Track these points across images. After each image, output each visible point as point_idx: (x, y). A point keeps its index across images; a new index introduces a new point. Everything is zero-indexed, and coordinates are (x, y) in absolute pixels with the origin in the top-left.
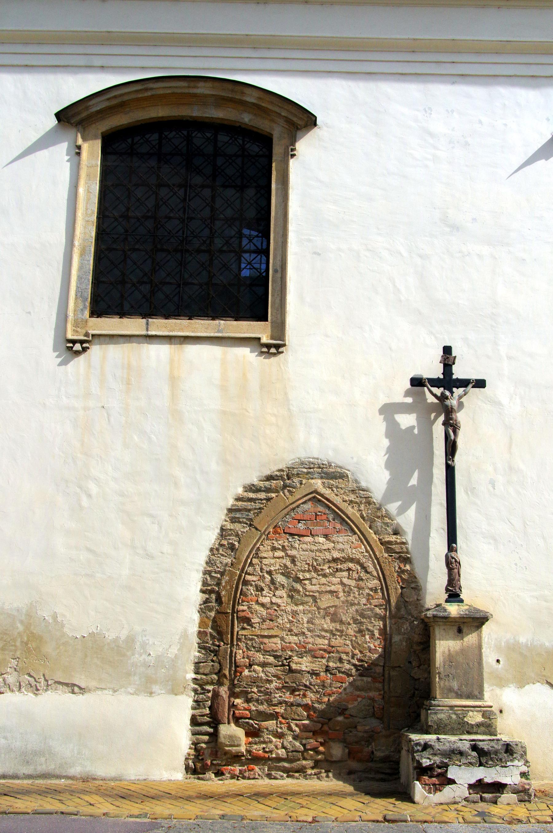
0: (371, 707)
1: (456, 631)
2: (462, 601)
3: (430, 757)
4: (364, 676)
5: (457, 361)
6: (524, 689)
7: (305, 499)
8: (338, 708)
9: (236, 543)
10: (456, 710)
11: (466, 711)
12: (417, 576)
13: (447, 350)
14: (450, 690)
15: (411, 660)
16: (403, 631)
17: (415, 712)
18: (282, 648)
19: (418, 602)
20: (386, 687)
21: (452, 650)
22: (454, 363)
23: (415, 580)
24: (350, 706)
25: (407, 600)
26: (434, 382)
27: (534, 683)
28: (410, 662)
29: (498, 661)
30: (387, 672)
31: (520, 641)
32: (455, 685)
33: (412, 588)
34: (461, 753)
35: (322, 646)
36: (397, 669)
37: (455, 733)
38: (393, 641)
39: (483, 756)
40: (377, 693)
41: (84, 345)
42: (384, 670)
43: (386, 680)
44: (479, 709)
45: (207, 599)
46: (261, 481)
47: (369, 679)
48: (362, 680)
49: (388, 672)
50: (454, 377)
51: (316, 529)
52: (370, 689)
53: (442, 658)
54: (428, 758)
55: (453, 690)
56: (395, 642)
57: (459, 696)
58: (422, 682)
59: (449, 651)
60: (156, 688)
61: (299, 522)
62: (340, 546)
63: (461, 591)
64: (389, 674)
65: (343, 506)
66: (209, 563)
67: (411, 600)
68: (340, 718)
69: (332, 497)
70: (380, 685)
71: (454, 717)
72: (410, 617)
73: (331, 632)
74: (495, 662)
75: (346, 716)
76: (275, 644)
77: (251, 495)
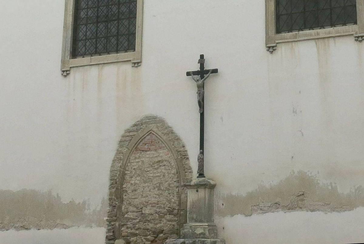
1: (196, 191)
4: (170, 215)
5: (198, 61)
7: (148, 133)
9: (122, 157)
12: (191, 166)
13: (202, 57)
14: (193, 219)
18: (140, 203)
24: (165, 229)
27: (238, 214)
29: (223, 204)
32: (195, 216)
36: (183, 210)
41: (68, 72)
42: (178, 211)
45: (112, 183)
46: (131, 127)
47: (173, 216)
48: (170, 217)
50: (199, 70)
60: (93, 225)
61: (146, 145)
66: (112, 166)
69: (158, 132)
71: (191, 231)
73: (158, 195)
76: (136, 202)
77: (128, 134)
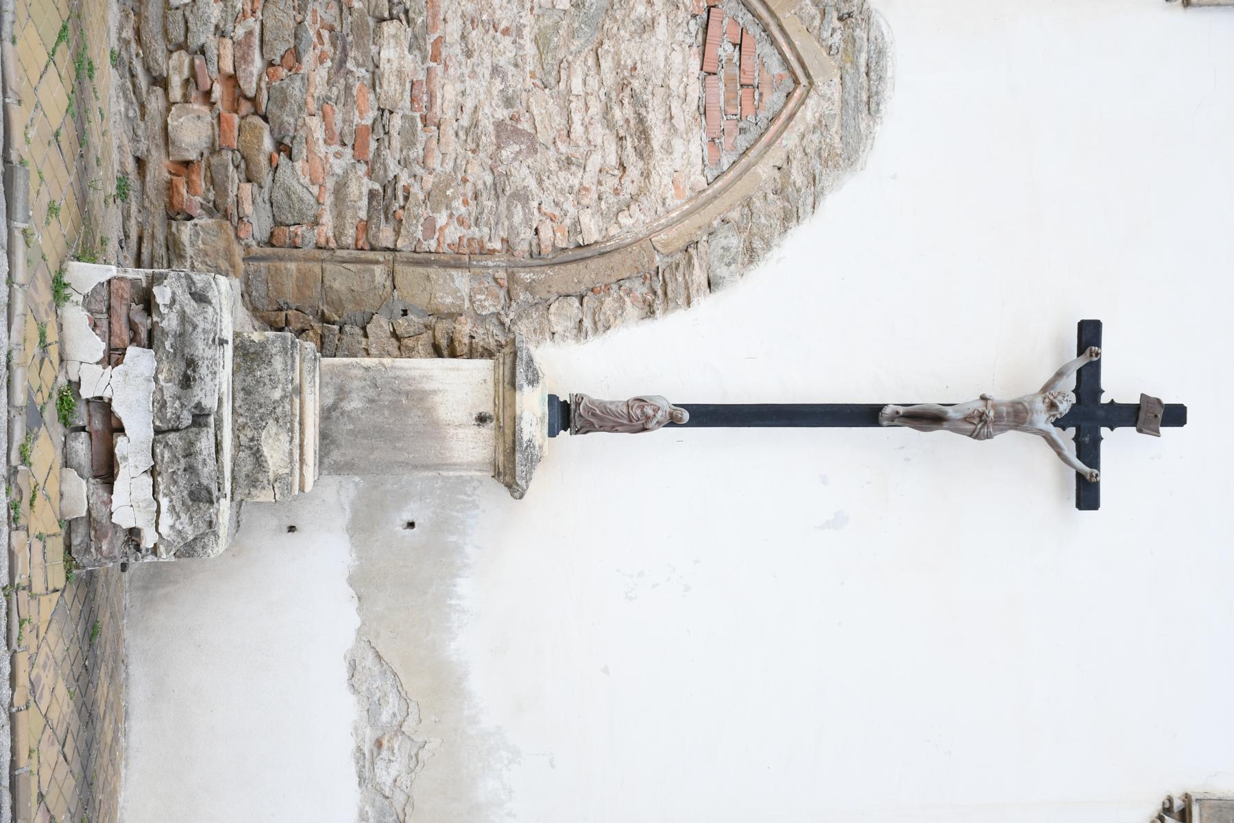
0: (297, 220)
1: (482, 409)
2: (552, 433)
3: (177, 306)
6: (346, 586)
8: (294, 138)
10: (292, 400)
11: (292, 425)
13: (1176, 415)
15: (411, 316)
16: (479, 297)
17: (287, 323)
19: (547, 335)
20: (344, 253)
21: (437, 399)
22: (1140, 431)
23: (601, 329)
25: (552, 309)
26: (1089, 378)
28: (405, 313)
29: (411, 525)
30: (379, 256)
31: (458, 580)
33: (581, 321)
34: (186, 382)
35: (439, 101)
36: (388, 283)
37: (240, 376)
38: (454, 272)
39: (181, 425)
40: (330, 234)
42: (388, 249)
43: (362, 255)
44: (297, 457)
47: (363, 214)
49: (381, 259)
51: (719, 89)
52: (339, 216)
53: (416, 373)
54: (173, 301)
55: (341, 400)
56: (452, 277)
57: (327, 414)
58: (359, 343)
59: (434, 392)
61: (735, 45)
62: (678, 144)
63: (577, 432)
64: (377, 262)
65: (776, 156)
67: (552, 318)
68: (268, 144)
69: (798, 126)
70: (350, 241)
72: (512, 316)
74: (408, 517)
75: (276, 155)
